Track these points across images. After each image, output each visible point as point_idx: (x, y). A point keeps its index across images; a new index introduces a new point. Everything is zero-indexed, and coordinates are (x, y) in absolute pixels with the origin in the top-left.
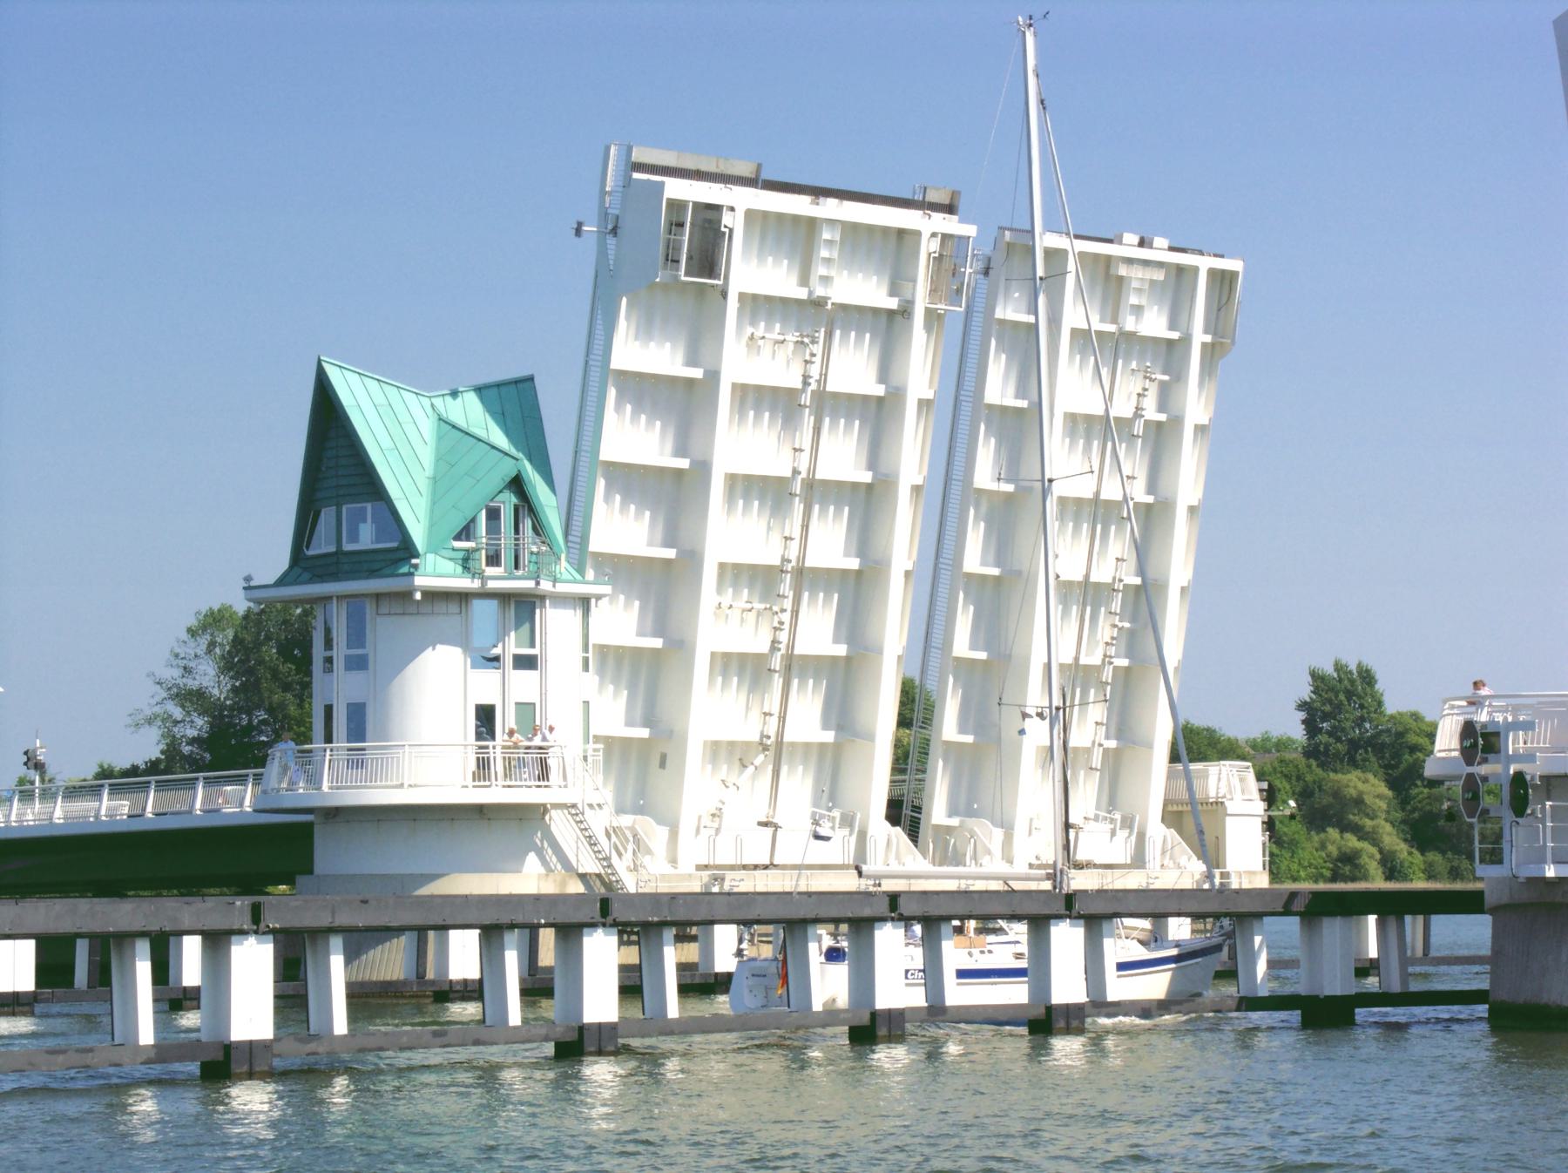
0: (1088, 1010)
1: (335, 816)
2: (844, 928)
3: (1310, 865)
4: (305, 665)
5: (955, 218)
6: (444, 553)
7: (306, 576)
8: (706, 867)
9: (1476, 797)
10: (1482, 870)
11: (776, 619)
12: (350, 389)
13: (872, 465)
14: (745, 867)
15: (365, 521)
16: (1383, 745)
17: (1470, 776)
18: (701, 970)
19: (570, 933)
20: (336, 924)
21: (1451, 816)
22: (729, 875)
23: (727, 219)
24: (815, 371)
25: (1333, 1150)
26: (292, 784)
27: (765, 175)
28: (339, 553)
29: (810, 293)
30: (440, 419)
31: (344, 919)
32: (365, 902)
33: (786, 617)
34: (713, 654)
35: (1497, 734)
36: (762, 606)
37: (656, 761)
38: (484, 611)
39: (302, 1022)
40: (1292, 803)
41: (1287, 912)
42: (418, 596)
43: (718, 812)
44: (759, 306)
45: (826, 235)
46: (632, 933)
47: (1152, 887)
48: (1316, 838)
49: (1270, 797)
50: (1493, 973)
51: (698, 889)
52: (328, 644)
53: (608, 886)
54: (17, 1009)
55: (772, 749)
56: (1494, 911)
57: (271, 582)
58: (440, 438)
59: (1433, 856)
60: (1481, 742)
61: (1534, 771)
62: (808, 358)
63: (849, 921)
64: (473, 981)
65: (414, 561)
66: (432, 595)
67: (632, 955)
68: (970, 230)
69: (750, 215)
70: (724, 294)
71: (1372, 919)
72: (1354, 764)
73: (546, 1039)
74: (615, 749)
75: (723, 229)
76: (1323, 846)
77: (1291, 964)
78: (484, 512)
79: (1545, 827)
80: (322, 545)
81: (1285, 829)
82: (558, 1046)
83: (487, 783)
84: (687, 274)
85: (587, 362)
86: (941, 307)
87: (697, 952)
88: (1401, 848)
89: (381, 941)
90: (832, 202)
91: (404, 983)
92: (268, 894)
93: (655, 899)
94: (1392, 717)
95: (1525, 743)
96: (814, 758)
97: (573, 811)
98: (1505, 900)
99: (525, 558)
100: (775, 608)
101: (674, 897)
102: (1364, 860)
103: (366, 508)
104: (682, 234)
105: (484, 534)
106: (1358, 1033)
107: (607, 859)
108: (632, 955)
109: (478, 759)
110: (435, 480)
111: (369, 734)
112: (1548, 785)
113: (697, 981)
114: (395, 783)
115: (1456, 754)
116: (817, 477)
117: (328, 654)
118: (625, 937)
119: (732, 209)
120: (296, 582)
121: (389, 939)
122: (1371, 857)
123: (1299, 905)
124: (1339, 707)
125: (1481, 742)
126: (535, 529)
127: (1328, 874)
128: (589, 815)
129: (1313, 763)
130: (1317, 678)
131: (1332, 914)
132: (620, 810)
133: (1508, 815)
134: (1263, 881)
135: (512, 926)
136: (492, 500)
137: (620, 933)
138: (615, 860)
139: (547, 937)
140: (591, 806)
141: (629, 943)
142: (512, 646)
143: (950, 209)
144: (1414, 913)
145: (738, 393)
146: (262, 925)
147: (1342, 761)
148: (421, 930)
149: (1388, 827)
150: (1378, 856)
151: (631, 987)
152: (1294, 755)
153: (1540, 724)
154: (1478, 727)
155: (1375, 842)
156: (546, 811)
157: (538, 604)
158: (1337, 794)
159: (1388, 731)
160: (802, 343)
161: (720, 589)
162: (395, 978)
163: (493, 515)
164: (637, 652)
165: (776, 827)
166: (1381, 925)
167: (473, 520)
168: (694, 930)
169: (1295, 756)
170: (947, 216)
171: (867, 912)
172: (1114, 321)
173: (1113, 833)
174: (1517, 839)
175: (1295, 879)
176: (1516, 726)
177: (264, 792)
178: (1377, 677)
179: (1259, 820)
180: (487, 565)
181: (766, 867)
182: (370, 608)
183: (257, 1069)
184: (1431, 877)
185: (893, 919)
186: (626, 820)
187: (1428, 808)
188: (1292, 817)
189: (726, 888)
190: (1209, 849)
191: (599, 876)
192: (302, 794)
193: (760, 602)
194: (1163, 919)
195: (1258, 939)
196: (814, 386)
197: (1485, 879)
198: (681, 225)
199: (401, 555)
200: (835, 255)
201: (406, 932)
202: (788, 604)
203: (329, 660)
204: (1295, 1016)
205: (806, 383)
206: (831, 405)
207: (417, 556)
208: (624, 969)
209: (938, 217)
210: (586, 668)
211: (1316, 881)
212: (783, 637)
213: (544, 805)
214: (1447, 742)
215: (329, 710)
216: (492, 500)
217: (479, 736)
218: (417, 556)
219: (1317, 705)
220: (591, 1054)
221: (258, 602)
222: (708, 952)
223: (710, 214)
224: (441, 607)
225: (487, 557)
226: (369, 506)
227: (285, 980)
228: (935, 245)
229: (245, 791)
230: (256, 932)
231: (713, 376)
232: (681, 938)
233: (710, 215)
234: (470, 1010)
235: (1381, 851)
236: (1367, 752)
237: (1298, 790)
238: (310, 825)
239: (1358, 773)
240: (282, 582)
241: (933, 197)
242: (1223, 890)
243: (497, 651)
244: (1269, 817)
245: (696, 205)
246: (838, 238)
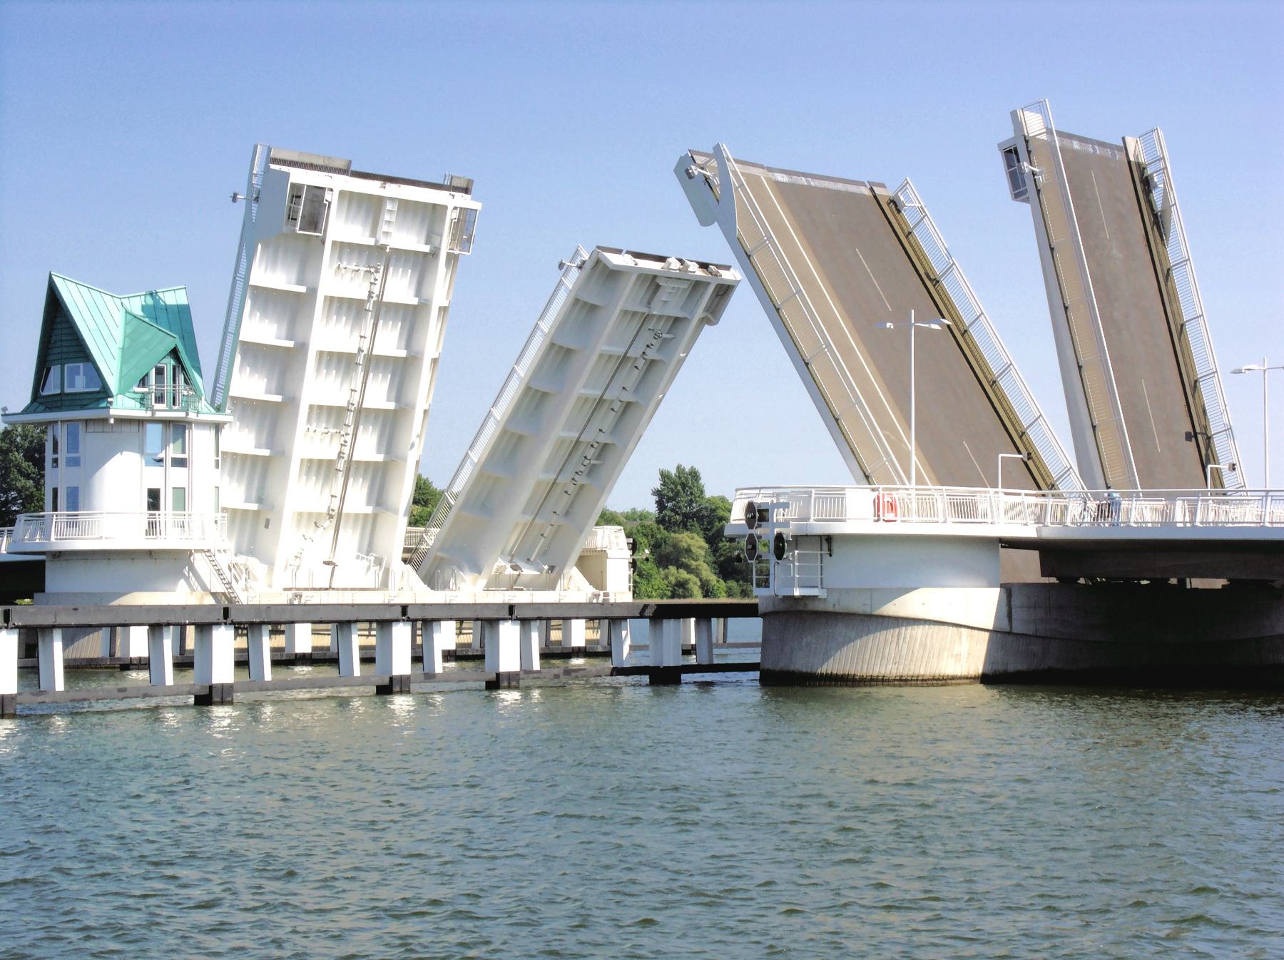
0: (522, 675)
1: (59, 556)
2: (374, 625)
3: (659, 588)
4: (40, 464)
5: (468, 197)
6: (127, 394)
7: (42, 408)
8: (290, 589)
9: (754, 548)
10: (757, 591)
11: (343, 439)
12: (70, 294)
13: (408, 346)
14: (315, 589)
15: (78, 374)
16: (703, 516)
17: (751, 536)
18: (287, 651)
19: (204, 628)
20: (57, 623)
21: (738, 559)
22: (304, 594)
23: (328, 196)
24: (376, 290)
26: (33, 536)
27: (353, 168)
28: (62, 394)
29: (376, 241)
30: (127, 312)
31: (63, 619)
32: (76, 609)
33: (349, 438)
34: (302, 460)
35: (767, 510)
36: (334, 431)
37: (263, 523)
38: (154, 431)
39: (35, 685)
40: (647, 551)
41: (642, 616)
42: (112, 421)
43: (299, 555)
44: (344, 248)
45: (389, 206)
46: (244, 628)
47: (562, 601)
48: (662, 572)
49: (634, 547)
50: (762, 653)
51: (285, 602)
52: (55, 450)
53: (230, 600)
54: (141, 667)
55: (335, 518)
56: (764, 616)
57: (20, 411)
58: (127, 324)
59: (732, 583)
60: (757, 515)
61: (788, 532)
62: (373, 281)
63: (378, 622)
64: (145, 658)
65: (110, 399)
66: (122, 421)
67: (242, 642)
68: (477, 205)
69: (342, 193)
70: (323, 242)
71: (693, 620)
72: (686, 527)
73: (189, 693)
74: (235, 515)
75: (325, 202)
76: (667, 577)
77: (645, 647)
78: (154, 370)
79: (794, 565)
80: (51, 389)
81: (644, 567)
82: (197, 698)
83: (155, 537)
84: (300, 229)
85: (235, 278)
86: (456, 252)
87: (284, 640)
88: (713, 578)
89: (87, 634)
90: (405, 188)
91: (102, 659)
92: (16, 604)
93: (258, 608)
94: (709, 500)
95: (784, 515)
96: (360, 522)
97: (208, 554)
98: (770, 609)
99: (179, 398)
100: (343, 433)
101: (269, 607)
102: (691, 585)
103: (79, 367)
104: (299, 205)
105: (154, 383)
106: (684, 688)
107: (229, 583)
108: (242, 642)
109: (149, 523)
110: (123, 349)
111: (81, 505)
112: (797, 541)
113: (284, 658)
114: (96, 536)
115: (744, 522)
116: (374, 353)
117: (55, 456)
118: (240, 631)
119: (332, 190)
120: (35, 412)
121: (92, 632)
122: (696, 583)
123: (649, 612)
124: (677, 494)
125: (757, 515)
126: (186, 382)
127: (669, 594)
128: (218, 557)
129: (662, 527)
130: (665, 476)
131: (669, 617)
132: (238, 552)
133: (773, 559)
134: (628, 597)
135: (168, 624)
136: (159, 363)
137: (236, 629)
138: (234, 584)
139: (191, 630)
140: (219, 551)
141: (242, 635)
142: (172, 452)
143: (466, 190)
144: (718, 617)
145: (328, 303)
146: (10, 624)
147: (679, 526)
148: (113, 627)
149: (705, 566)
150: (699, 583)
151: (242, 663)
152: (650, 523)
153: (792, 504)
154: (756, 507)
155: (698, 575)
156: (191, 554)
157: (187, 426)
158: (675, 546)
159: (706, 508)
160: (370, 271)
161: (309, 421)
162: (96, 657)
163: (160, 372)
164: (255, 458)
165: (335, 565)
166: (697, 623)
167: (147, 375)
168: (282, 627)
169: (651, 522)
170: (464, 195)
171: (388, 616)
173: (369, 568)
174: (777, 571)
175: (649, 597)
176: (779, 505)
177: (14, 542)
178: (701, 475)
179: (627, 562)
180: (156, 402)
181: (326, 589)
182: (81, 427)
183: (7, 712)
184: (730, 595)
185: (404, 621)
186: (241, 559)
187: (729, 554)
188: (647, 560)
189: (303, 602)
190: (596, 577)
191: (224, 594)
192: (38, 542)
193: (334, 428)
194: (127, 628)
195: (624, 633)
196: (375, 299)
197: (759, 595)
198: (299, 197)
199: (102, 395)
200: (393, 219)
201: (103, 628)
202: (350, 430)
203: (55, 461)
204: (646, 679)
205: (370, 296)
206: (384, 310)
207: (112, 396)
208: (238, 651)
209: (458, 195)
210: (217, 467)
211: (662, 598)
212: (346, 450)
213: (190, 551)
214: (737, 515)
215: (55, 491)
216: (159, 363)
218: (112, 396)
219: (665, 492)
220: (397, 693)
221: (10, 424)
222: (291, 640)
224: (126, 428)
225: (156, 398)
226: (81, 365)
227: (27, 657)
228: (455, 215)
229: (2, 541)
230: (6, 628)
231: (313, 292)
232: (274, 632)
233: (318, 192)
234: (142, 675)
235: (701, 580)
236: (693, 521)
237: (652, 543)
238: (43, 562)
239: (688, 533)
240: (26, 411)
241: (456, 183)
242: (605, 604)
243: (161, 455)
244: (633, 560)
245: (309, 186)
246: (396, 209)
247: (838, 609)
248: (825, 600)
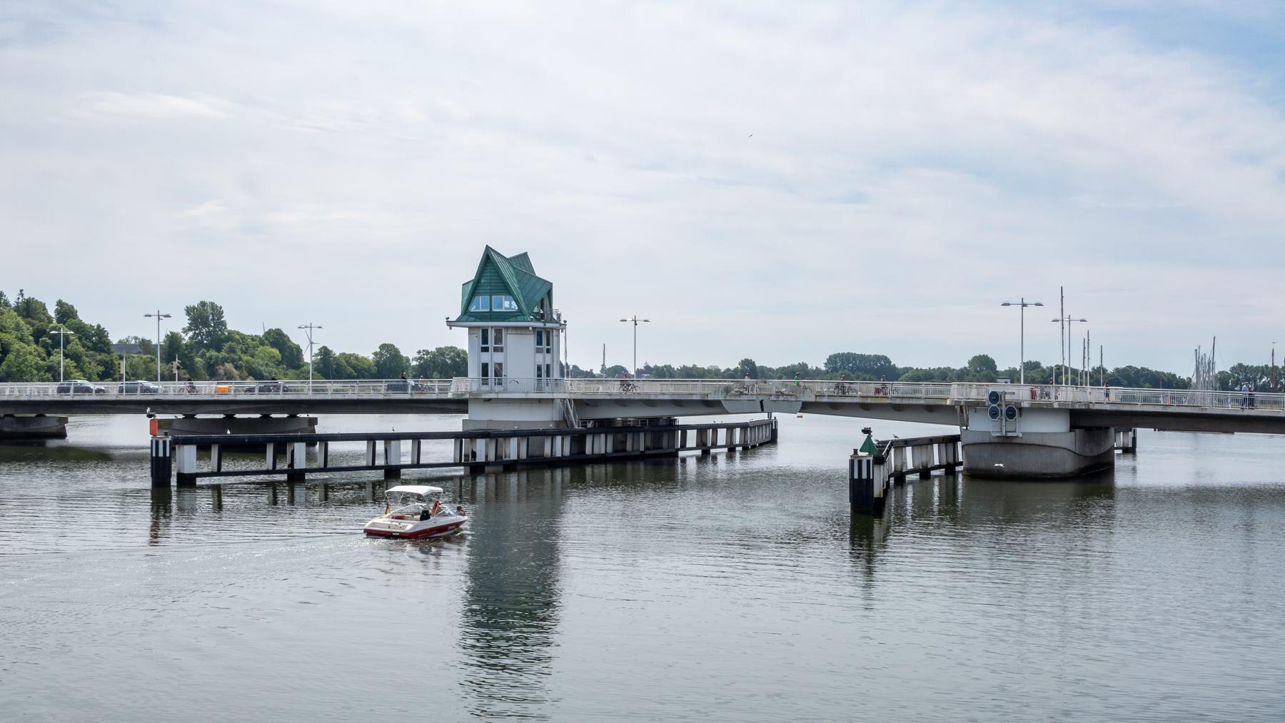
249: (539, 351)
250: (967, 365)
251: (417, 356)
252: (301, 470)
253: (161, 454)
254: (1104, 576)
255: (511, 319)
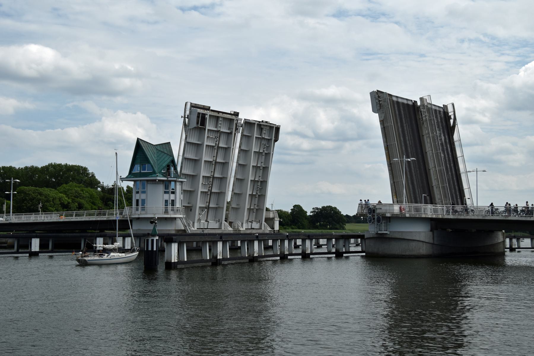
23: (206, 116)
25: (519, 300)
70: (205, 129)
172: (261, 135)
205: (216, 145)
217: (165, 205)
223: (204, 115)
247: (393, 237)
248: (389, 234)
249: (165, 192)
250: (40, 167)
251: (312, 210)
252: (36, 252)
253: (150, 249)
254: (528, 292)
255: (149, 176)
